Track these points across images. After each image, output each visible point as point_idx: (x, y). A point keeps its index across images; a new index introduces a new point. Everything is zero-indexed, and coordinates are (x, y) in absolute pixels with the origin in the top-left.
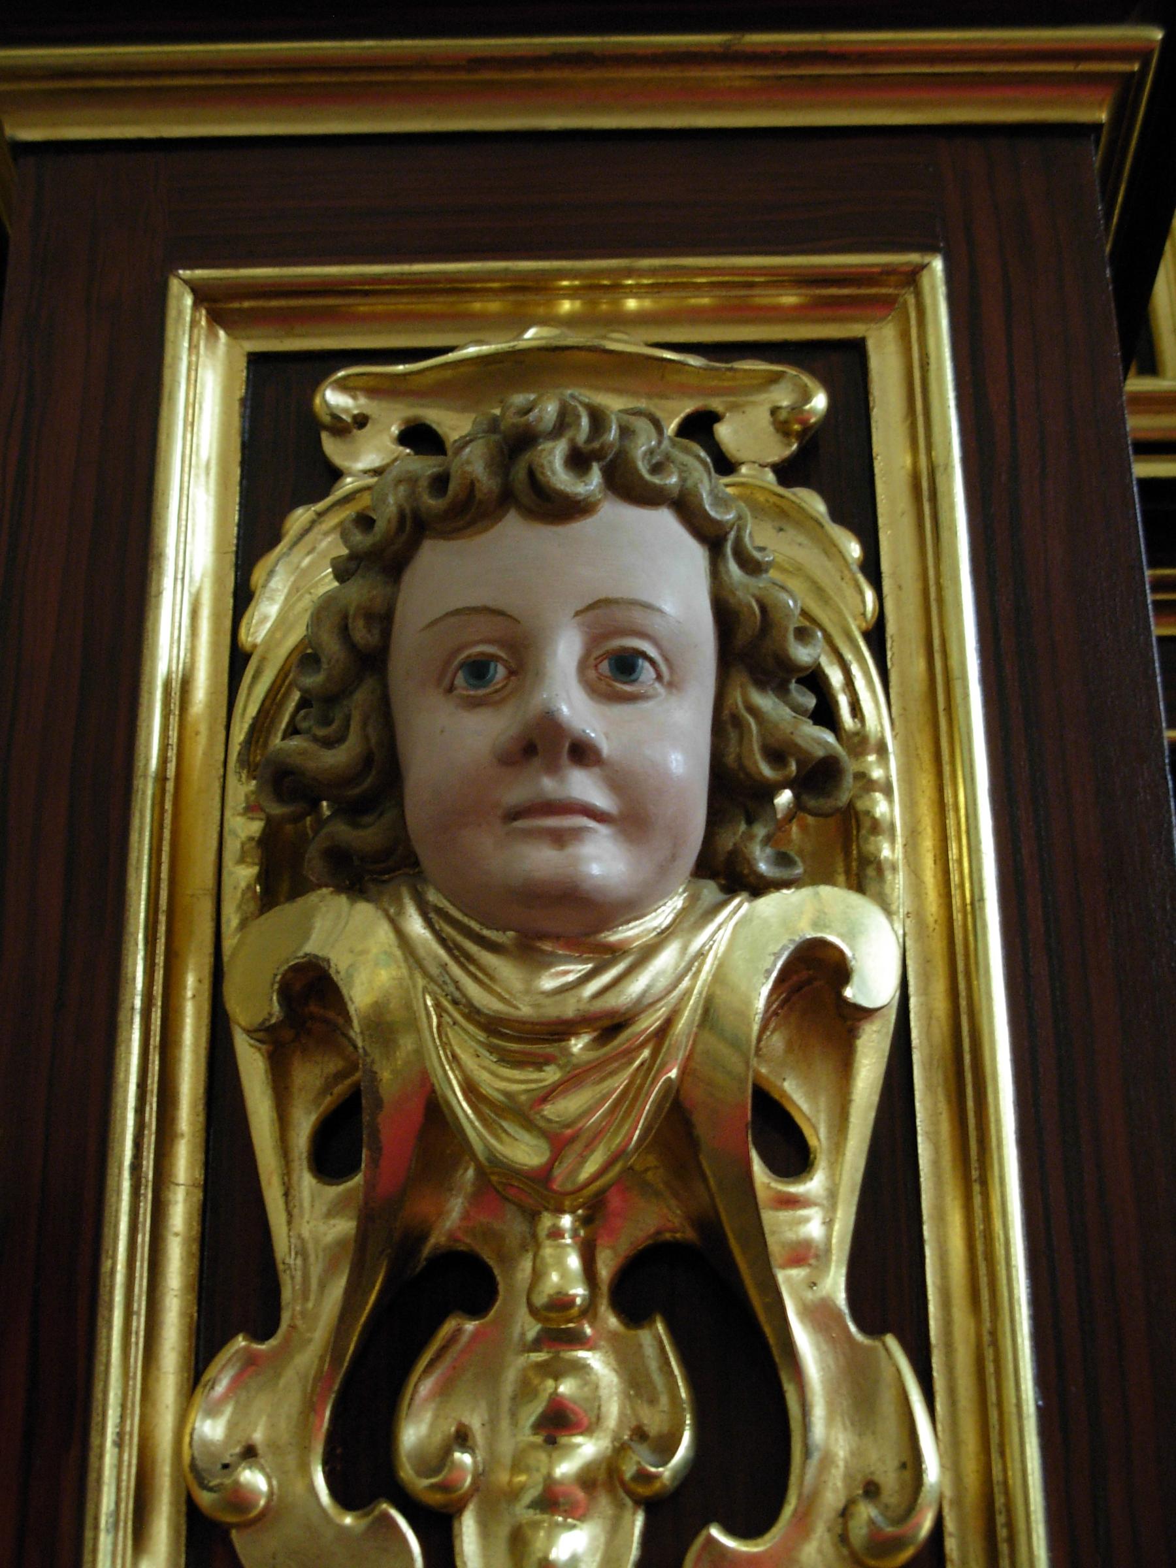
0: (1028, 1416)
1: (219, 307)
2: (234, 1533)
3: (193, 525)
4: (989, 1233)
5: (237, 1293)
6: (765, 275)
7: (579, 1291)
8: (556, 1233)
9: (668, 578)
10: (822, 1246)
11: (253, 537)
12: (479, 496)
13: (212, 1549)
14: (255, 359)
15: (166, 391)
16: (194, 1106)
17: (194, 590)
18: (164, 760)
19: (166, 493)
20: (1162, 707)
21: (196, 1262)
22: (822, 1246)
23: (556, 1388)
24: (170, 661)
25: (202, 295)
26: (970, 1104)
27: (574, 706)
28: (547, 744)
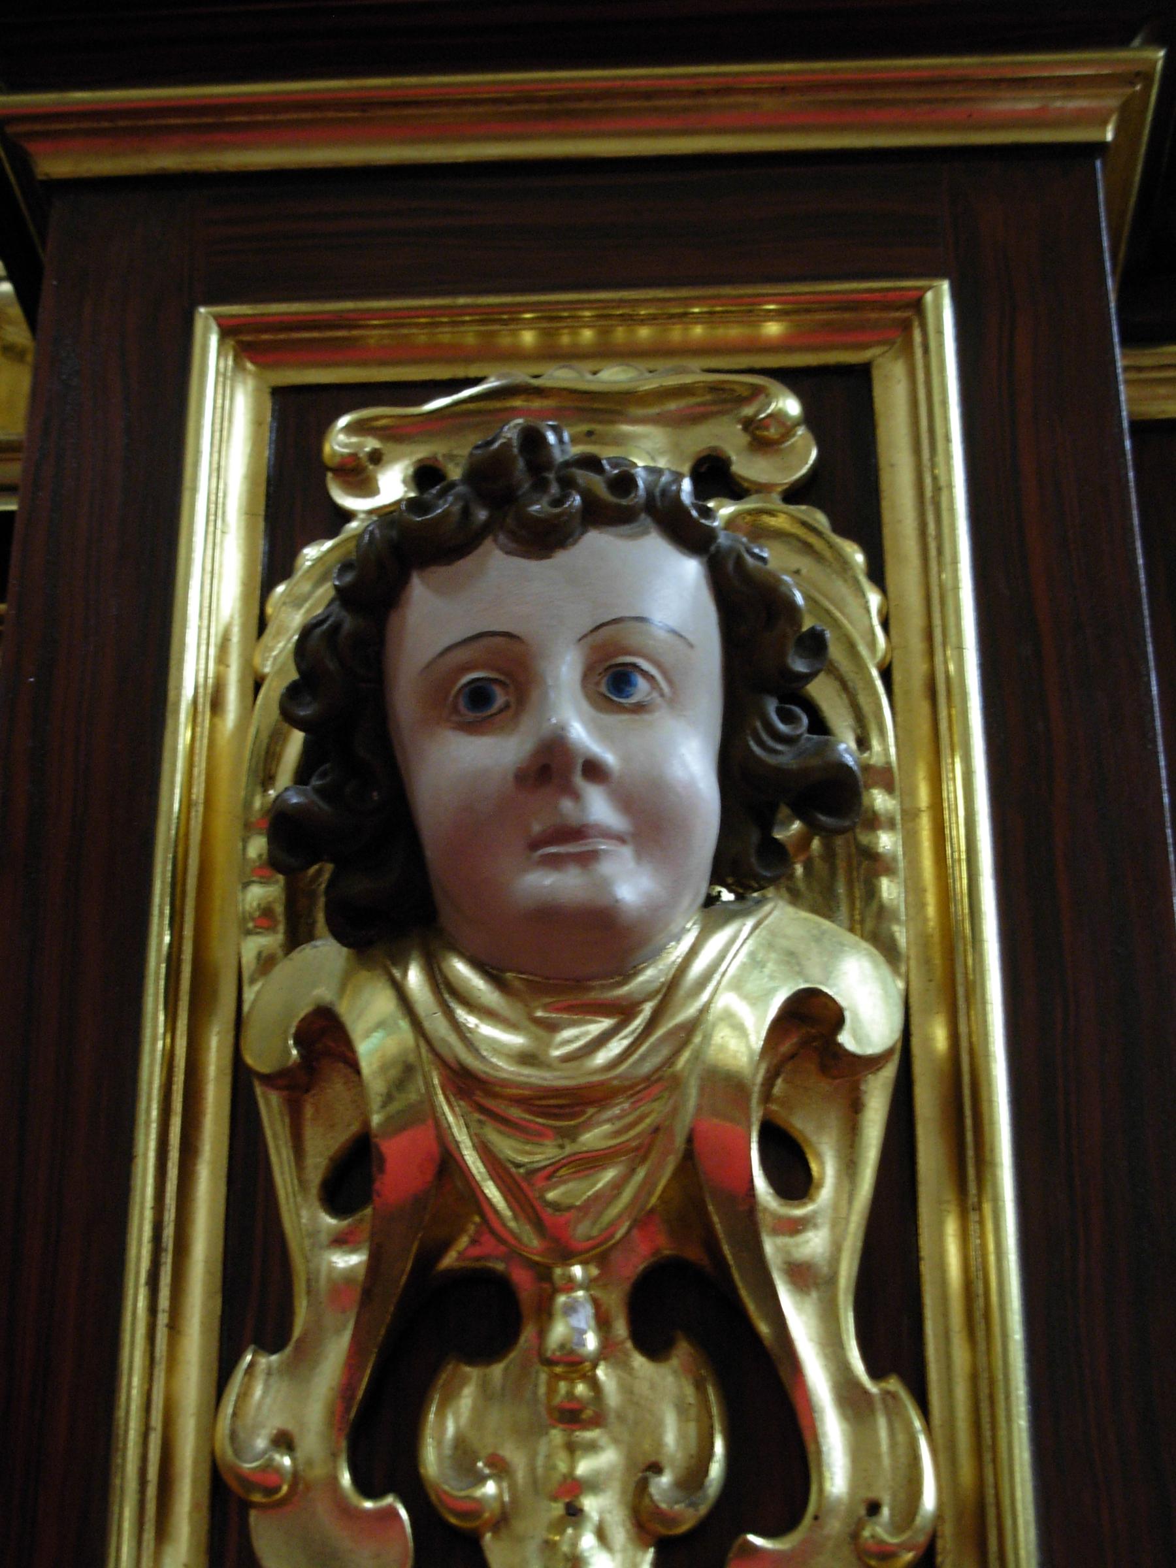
0: (1017, 1397)
1: (246, 344)
2: (253, 1515)
3: (225, 497)
4: (983, 1249)
5: (257, 1307)
6: (974, 964)
7: (591, 1342)
8: (570, 1285)
9: (672, 592)
10: (825, 1270)
11: (274, 564)
12: (580, 1367)
13: (230, 1504)
14: (279, 393)
15: (170, 707)
16: (209, 1272)
17: (221, 628)
18: (188, 803)
19: (189, 560)
20: (1162, 763)
21: (205, 1511)
22: (825, 1270)
23: (572, 1467)
24: (196, 688)
25: (228, 331)
26: (969, 1136)
27: (581, 731)
28: (553, 768)
